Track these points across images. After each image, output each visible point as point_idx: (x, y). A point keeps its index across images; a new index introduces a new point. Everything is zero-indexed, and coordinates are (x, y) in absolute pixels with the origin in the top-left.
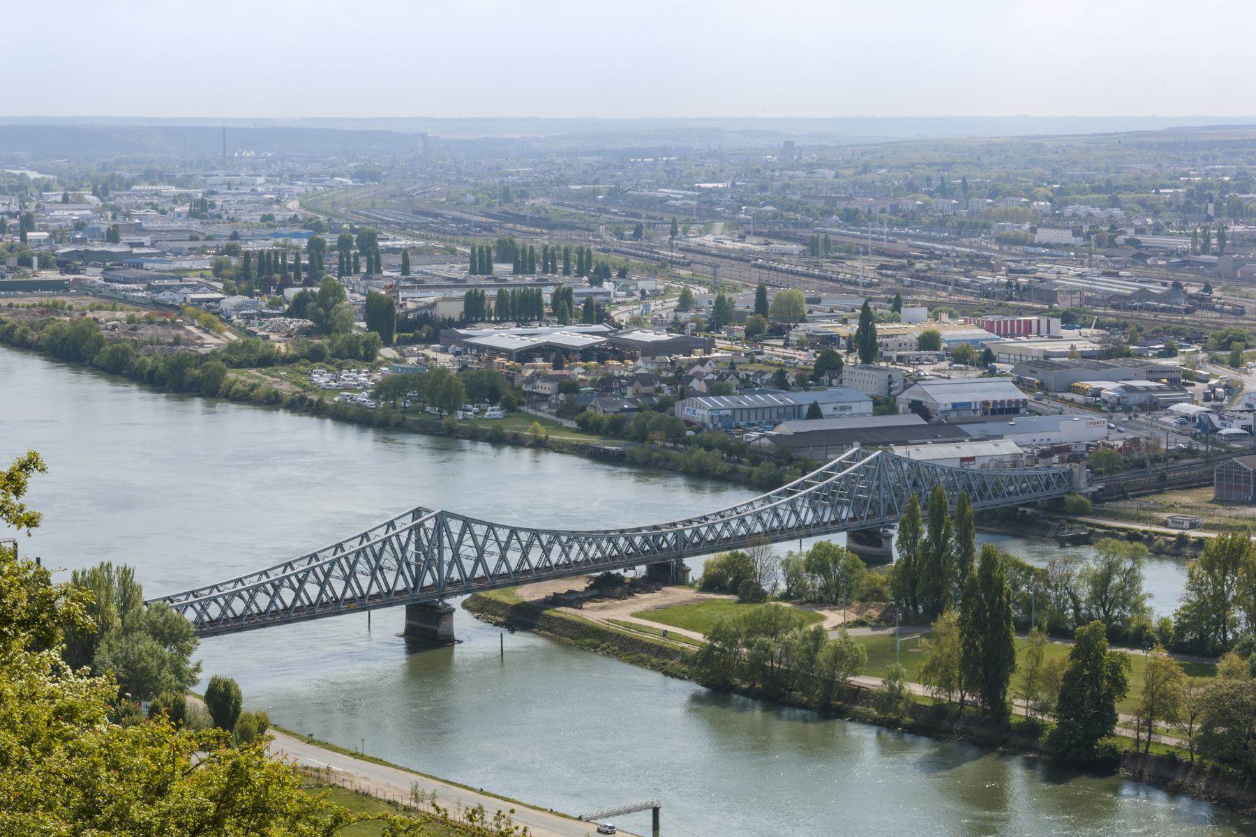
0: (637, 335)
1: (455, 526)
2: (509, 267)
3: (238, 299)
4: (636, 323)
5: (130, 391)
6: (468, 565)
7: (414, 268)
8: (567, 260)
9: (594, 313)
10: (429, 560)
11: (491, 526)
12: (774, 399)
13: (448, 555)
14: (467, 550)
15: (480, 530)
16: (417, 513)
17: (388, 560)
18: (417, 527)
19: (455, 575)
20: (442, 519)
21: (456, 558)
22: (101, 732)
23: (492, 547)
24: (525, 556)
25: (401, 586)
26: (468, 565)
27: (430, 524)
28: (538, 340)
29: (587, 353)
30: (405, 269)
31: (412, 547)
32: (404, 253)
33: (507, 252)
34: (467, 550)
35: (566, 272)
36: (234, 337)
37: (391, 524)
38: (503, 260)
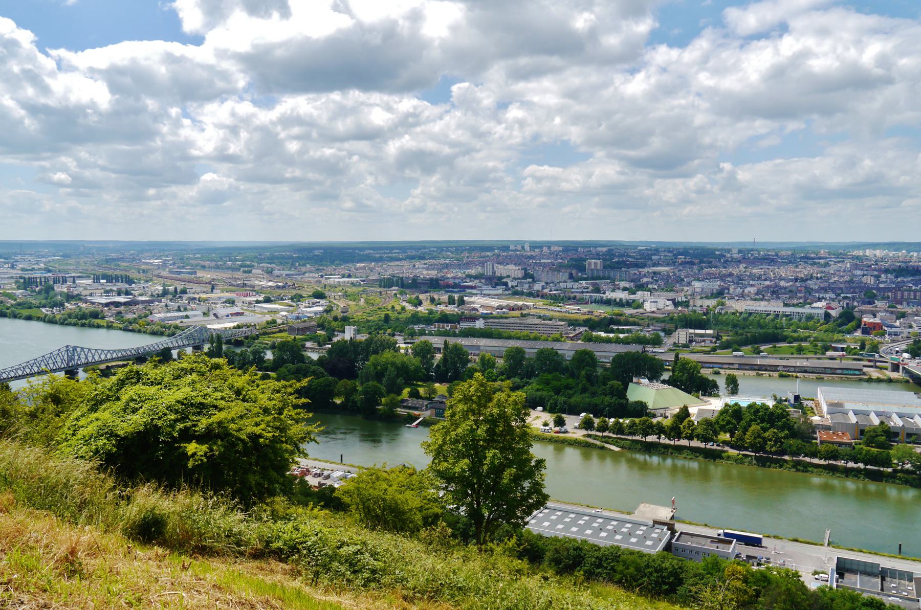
0: (141, 298)
1: (79, 350)
2: (105, 281)
3: (21, 291)
4: (141, 295)
5: (146, 59)
6: (59, 364)
7: (77, 281)
8: (122, 278)
9: (127, 293)
10: (71, 359)
11: (89, 350)
12: (176, 314)
13: (76, 358)
14: (83, 356)
15: (86, 351)
16: (67, 346)
17: (58, 360)
18: (67, 351)
19: (79, 363)
20: (75, 348)
21: (79, 357)
22: (289, 508)
23: (90, 354)
24: (106, 356)
25: (63, 366)
26: (59, 364)
27: (71, 349)
28: (110, 300)
29: (125, 304)
30: (74, 282)
31: (66, 356)
32: (74, 277)
33: (105, 277)
34: (83, 356)
35: (122, 282)
36: (153, 144)
37: (59, 350)
38: (103, 279)
